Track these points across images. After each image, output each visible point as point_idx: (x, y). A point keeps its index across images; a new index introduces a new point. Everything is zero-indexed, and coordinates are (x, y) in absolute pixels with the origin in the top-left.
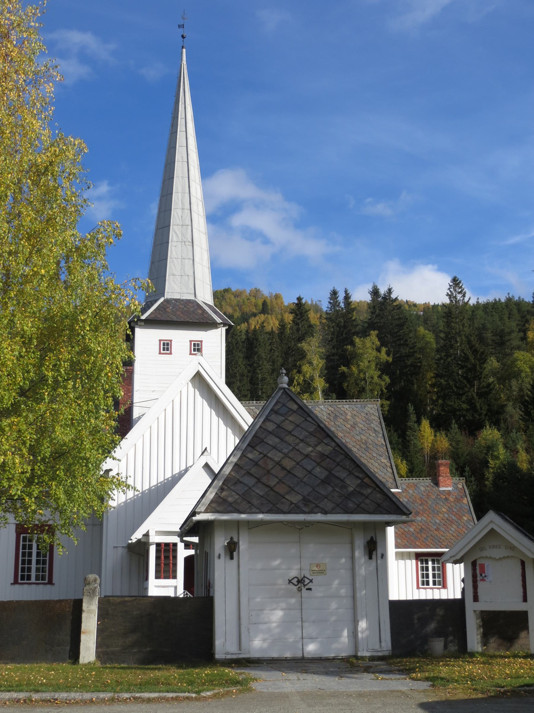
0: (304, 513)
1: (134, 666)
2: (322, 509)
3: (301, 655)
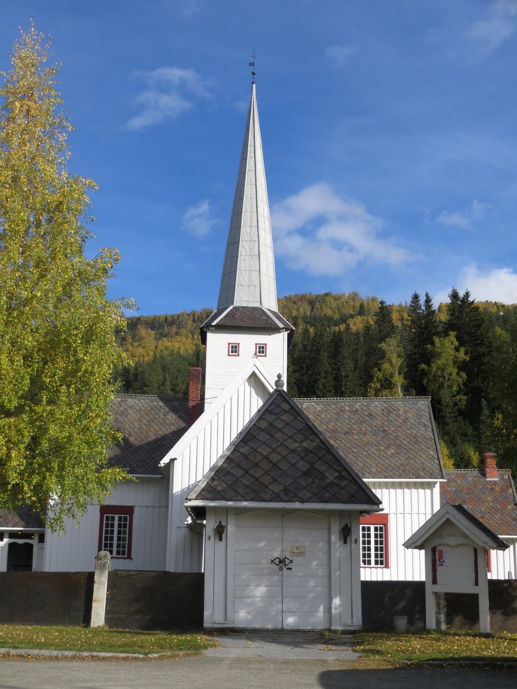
0: (283, 501)
1: (138, 631)
2: (301, 498)
3: (281, 627)
